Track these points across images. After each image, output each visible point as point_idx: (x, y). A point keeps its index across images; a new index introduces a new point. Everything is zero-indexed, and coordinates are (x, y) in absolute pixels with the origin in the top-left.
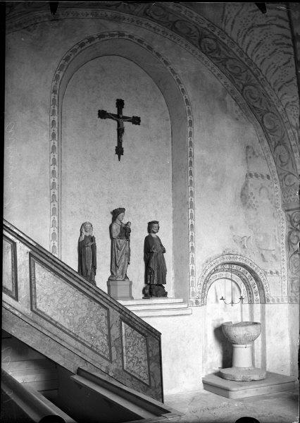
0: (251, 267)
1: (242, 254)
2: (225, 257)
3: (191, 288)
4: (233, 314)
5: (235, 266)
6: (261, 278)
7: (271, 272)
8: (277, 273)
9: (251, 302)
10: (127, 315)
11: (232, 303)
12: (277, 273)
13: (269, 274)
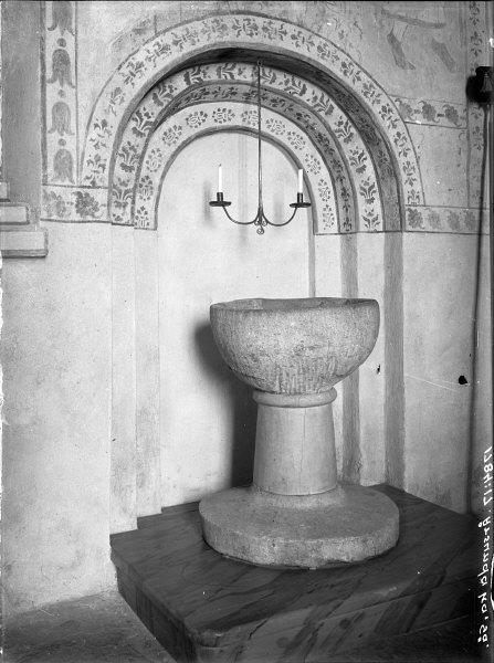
3: (53, 138)
5: (281, 77)
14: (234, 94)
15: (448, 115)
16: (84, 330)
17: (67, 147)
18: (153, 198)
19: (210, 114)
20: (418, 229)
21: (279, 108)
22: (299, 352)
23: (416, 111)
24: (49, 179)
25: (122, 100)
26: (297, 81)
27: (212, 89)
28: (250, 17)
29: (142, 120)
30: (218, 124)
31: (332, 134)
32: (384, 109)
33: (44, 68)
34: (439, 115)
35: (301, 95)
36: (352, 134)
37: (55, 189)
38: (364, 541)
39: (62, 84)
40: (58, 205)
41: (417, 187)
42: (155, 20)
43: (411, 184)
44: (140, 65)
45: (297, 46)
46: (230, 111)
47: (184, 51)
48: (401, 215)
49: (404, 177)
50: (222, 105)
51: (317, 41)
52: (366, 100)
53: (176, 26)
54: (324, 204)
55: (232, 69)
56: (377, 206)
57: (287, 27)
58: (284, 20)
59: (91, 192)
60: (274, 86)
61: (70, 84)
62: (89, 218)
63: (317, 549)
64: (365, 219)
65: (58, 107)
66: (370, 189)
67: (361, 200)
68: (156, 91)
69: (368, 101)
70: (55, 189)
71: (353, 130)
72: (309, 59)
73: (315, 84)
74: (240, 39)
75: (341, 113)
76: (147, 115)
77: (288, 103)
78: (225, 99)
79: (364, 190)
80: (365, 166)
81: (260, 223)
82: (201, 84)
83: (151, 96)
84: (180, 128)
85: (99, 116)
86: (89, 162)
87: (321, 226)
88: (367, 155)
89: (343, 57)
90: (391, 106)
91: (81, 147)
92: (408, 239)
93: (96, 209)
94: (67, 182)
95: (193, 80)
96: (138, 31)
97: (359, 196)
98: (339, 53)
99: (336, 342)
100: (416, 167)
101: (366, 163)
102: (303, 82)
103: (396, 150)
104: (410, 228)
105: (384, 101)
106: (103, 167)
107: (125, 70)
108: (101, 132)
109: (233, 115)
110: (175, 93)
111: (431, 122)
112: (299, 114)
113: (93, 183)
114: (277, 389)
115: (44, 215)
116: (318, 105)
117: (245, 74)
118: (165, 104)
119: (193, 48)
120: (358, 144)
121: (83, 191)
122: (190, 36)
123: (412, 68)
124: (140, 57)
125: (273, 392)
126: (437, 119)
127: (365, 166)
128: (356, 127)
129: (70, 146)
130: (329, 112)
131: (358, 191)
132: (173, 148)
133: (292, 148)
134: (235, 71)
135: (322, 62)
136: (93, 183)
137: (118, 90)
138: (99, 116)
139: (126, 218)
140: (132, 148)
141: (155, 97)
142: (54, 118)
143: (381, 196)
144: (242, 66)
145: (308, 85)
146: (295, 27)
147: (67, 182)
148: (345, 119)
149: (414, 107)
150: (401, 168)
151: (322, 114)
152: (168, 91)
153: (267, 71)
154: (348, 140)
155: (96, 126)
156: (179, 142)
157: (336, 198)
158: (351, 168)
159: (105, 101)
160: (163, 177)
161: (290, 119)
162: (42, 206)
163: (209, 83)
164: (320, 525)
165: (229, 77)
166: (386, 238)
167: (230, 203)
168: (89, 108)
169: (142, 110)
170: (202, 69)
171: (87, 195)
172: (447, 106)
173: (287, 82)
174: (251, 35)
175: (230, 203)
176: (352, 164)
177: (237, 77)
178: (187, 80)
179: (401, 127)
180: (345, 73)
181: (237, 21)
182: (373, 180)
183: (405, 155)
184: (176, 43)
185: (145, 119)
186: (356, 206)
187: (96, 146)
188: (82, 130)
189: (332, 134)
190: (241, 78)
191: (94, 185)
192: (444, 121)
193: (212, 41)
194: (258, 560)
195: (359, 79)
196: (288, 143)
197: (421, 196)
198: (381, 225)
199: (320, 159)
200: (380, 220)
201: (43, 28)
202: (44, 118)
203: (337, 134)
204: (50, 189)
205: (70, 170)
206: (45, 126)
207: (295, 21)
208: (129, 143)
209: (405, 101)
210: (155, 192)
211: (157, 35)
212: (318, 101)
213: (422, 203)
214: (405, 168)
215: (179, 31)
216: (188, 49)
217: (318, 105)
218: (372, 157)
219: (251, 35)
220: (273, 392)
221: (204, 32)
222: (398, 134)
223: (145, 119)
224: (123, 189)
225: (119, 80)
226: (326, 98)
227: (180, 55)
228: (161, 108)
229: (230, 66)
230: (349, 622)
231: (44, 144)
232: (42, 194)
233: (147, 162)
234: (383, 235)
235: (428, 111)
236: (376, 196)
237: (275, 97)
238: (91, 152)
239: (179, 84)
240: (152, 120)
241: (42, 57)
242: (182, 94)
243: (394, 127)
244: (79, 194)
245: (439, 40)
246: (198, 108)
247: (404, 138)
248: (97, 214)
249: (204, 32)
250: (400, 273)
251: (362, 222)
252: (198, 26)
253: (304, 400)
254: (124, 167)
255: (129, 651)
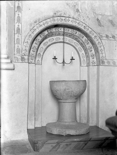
0: (85, 30)
1: (75, 17)
2: (56, 18)
3: (16, 45)
4: (75, 72)
5: (70, 30)
6: (96, 41)
7: (107, 36)
8: (113, 37)
9: (88, 65)
10: (87, 59)
11: (64, 62)
12: (113, 37)
13: (105, 38)
14: (60, 34)
15: (113, 37)
16: (22, 85)
17: (19, 47)
18: (41, 58)
19: (55, 39)
20: (104, 65)
21: (71, 37)
22: (65, 90)
23: (104, 37)
24: (15, 53)
25: (31, 37)
26: (74, 30)
27: (54, 33)
28: (61, 17)
29: (37, 41)
30: (57, 41)
31: (84, 43)
32: (95, 36)
33: (15, 31)
34: (110, 37)
35: (75, 34)
36: (89, 43)
37: (16, 56)
38: (76, 131)
39: (18, 34)
40: (17, 59)
41: (104, 55)
42: (39, 20)
43: (102, 54)
44: (35, 29)
45: (72, 23)
46: (59, 38)
47: (45, 26)
48: (100, 61)
49: (100, 52)
50: (57, 37)
51: (77, 21)
52: (90, 35)
53: (44, 21)
54: (83, 59)
55: (58, 29)
56: (95, 60)
57: (70, 19)
58: (69, 17)
59: (24, 56)
60: (69, 32)
61: (20, 34)
62: (24, 62)
63: (65, 131)
64: (92, 62)
65: (17, 39)
66: (93, 56)
67: (91, 58)
68: (40, 34)
69: (91, 35)
70: (16, 56)
71: (89, 42)
72: (75, 26)
73: (79, 31)
74: (58, 22)
75: (86, 38)
76: (38, 40)
77: (73, 36)
78: (58, 35)
79: (92, 56)
80: (92, 50)
81: (64, 63)
82: (51, 32)
83: (39, 36)
84: (48, 42)
85: (26, 41)
86: (24, 50)
87: (82, 65)
88: (92, 47)
89: (84, 25)
90: (97, 36)
91: (22, 47)
92: (91, 67)
93: (25, 60)
94: (19, 54)
95: (49, 32)
96: (35, 22)
97: (90, 57)
98: (83, 24)
99: (73, 88)
100: (104, 50)
101: (92, 49)
102: (76, 31)
103: (98, 46)
104: (102, 65)
105: (95, 34)
106: (27, 51)
107: (32, 31)
108: (26, 44)
109: (60, 39)
110: (45, 35)
111: (108, 39)
112: (76, 38)
113: (25, 54)
114: (62, 98)
115: (14, 61)
116: (80, 36)
117: (61, 30)
118: (43, 37)
119: (47, 25)
120: (90, 45)
121: (22, 56)
122: (47, 23)
123: (103, 26)
124: (35, 28)
125: (61, 99)
126: (109, 38)
127: (92, 50)
128: (90, 41)
129: (20, 47)
130: (83, 37)
131: (90, 56)
132: (46, 47)
133: (75, 46)
134: (59, 29)
135: (78, 26)
136: (25, 54)
137: (30, 35)
138: (26, 41)
139: (33, 62)
140: (35, 47)
141: (40, 36)
142: (17, 41)
143: (96, 57)
144: (61, 28)
145: (77, 31)
146: (72, 19)
147: (19, 54)
148: (87, 39)
149: (103, 36)
150: (99, 50)
151: (81, 38)
152: (43, 34)
153: (67, 29)
154: (87, 44)
155: (25, 43)
156: (47, 45)
157: (86, 58)
158: (88, 50)
159: (27, 37)
160: (44, 53)
161: (75, 40)
162: (14, 59)
163: (53, 32)
164: (68, 127)
165: (58, 31)
166: (97, 67)
167: (57, 59)
168: (24, 39)
169: (37, 39)
170: (51, 29)
171: (23, 57)
172: (112, 35)
173: (72, 31)
174: (61, 21)
175: (57, 59)
176: (89, 50)
177: (60, 31)
178: (48, 32)
179: (99, 40)
180: (85, 29)
181: (58, 18)
182: (94, 53)
183: (101, 47)
184: (43, 24)
185: (38, 41)
186: (89, 59)
187: (25, 47)
188: (22, 44)
189: (84, 43)
190: (61, 31)
191: (25, 55)
192: (112, 39)
193: (52, 23)
194: (54, 133)
195: (88, 30)
196: (74, 45)
197: (105, 57)
198: (96, 64)
199: (82, 48)
200: (96, 63)
201: (15, 23)
202: (14, 41)
203: (85, 43)
204: (15, 56)
205: (20, 52)
206: (15, 43)
207: (72, 17)
208: (34, 46)
209: (101, 34)
210: (41, 57)
211: (39, 23)
212: (80, 35)
213: (105, 58)
214: (100, 50)
215: (44, 22)
216: (46, 25)
217: (80, 36)
218: (94, 48)
219: (61, 21)
220: (61, 99)
221: (50, 21)
222: (99, 42)
223: (38, 41)
224: (33, 56)
225: (31, 33)
226: (82, 34)
227: (45, 26)
228: (41, 38)
229: (58, 28)
230: (68, 145)
231: (14, 47)
232: (14, 57)
233: (40, 50)
234: (96, 66)
235: (107, 36)
236: (95, 57)
237: (70, 34)
238: (24, 48)
239: (46, 33)
240: (40, 41)
241: (14, 29)
242: (47, 35)
243: (98, 41)
244: (22, 57)
245: (111, 19)
246: (52, 38)
247: (100, 43)
248: (25, 61)
249: (50, 21)
250: (99, 75)
251: (91, 63)
252: (49, 20)
253: (68, 101)
254: (33, 51)
255: (26, 151)
